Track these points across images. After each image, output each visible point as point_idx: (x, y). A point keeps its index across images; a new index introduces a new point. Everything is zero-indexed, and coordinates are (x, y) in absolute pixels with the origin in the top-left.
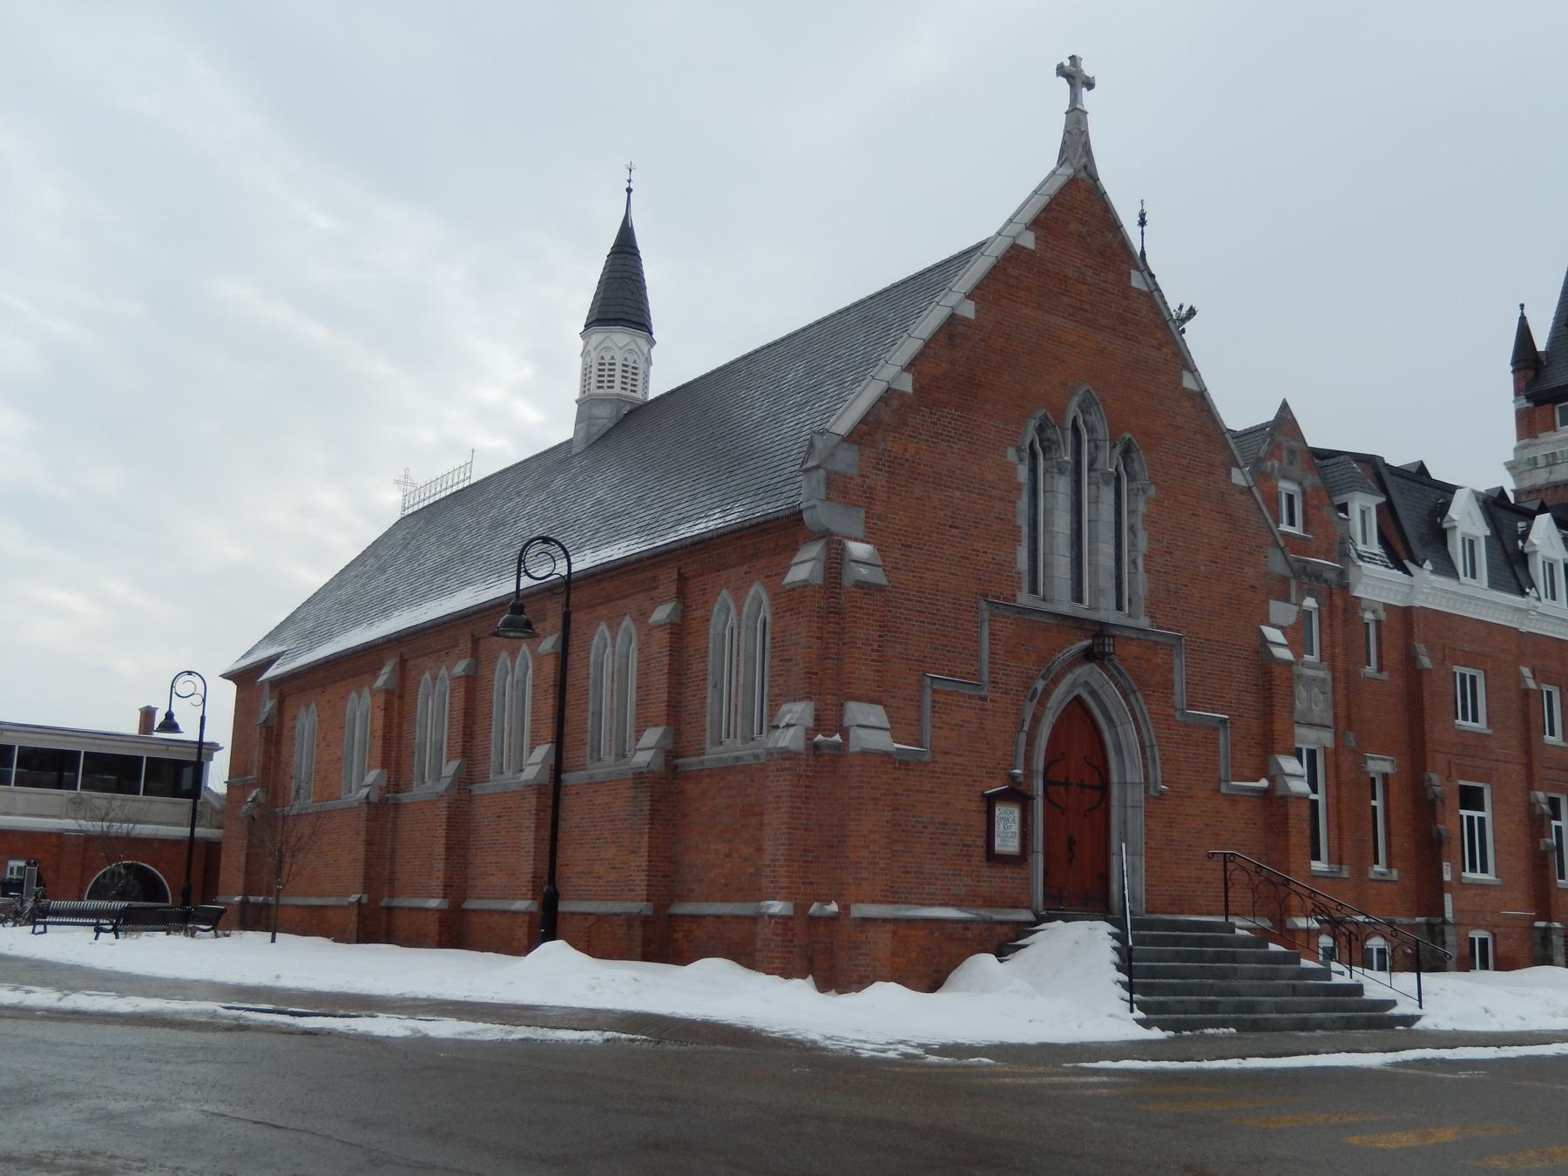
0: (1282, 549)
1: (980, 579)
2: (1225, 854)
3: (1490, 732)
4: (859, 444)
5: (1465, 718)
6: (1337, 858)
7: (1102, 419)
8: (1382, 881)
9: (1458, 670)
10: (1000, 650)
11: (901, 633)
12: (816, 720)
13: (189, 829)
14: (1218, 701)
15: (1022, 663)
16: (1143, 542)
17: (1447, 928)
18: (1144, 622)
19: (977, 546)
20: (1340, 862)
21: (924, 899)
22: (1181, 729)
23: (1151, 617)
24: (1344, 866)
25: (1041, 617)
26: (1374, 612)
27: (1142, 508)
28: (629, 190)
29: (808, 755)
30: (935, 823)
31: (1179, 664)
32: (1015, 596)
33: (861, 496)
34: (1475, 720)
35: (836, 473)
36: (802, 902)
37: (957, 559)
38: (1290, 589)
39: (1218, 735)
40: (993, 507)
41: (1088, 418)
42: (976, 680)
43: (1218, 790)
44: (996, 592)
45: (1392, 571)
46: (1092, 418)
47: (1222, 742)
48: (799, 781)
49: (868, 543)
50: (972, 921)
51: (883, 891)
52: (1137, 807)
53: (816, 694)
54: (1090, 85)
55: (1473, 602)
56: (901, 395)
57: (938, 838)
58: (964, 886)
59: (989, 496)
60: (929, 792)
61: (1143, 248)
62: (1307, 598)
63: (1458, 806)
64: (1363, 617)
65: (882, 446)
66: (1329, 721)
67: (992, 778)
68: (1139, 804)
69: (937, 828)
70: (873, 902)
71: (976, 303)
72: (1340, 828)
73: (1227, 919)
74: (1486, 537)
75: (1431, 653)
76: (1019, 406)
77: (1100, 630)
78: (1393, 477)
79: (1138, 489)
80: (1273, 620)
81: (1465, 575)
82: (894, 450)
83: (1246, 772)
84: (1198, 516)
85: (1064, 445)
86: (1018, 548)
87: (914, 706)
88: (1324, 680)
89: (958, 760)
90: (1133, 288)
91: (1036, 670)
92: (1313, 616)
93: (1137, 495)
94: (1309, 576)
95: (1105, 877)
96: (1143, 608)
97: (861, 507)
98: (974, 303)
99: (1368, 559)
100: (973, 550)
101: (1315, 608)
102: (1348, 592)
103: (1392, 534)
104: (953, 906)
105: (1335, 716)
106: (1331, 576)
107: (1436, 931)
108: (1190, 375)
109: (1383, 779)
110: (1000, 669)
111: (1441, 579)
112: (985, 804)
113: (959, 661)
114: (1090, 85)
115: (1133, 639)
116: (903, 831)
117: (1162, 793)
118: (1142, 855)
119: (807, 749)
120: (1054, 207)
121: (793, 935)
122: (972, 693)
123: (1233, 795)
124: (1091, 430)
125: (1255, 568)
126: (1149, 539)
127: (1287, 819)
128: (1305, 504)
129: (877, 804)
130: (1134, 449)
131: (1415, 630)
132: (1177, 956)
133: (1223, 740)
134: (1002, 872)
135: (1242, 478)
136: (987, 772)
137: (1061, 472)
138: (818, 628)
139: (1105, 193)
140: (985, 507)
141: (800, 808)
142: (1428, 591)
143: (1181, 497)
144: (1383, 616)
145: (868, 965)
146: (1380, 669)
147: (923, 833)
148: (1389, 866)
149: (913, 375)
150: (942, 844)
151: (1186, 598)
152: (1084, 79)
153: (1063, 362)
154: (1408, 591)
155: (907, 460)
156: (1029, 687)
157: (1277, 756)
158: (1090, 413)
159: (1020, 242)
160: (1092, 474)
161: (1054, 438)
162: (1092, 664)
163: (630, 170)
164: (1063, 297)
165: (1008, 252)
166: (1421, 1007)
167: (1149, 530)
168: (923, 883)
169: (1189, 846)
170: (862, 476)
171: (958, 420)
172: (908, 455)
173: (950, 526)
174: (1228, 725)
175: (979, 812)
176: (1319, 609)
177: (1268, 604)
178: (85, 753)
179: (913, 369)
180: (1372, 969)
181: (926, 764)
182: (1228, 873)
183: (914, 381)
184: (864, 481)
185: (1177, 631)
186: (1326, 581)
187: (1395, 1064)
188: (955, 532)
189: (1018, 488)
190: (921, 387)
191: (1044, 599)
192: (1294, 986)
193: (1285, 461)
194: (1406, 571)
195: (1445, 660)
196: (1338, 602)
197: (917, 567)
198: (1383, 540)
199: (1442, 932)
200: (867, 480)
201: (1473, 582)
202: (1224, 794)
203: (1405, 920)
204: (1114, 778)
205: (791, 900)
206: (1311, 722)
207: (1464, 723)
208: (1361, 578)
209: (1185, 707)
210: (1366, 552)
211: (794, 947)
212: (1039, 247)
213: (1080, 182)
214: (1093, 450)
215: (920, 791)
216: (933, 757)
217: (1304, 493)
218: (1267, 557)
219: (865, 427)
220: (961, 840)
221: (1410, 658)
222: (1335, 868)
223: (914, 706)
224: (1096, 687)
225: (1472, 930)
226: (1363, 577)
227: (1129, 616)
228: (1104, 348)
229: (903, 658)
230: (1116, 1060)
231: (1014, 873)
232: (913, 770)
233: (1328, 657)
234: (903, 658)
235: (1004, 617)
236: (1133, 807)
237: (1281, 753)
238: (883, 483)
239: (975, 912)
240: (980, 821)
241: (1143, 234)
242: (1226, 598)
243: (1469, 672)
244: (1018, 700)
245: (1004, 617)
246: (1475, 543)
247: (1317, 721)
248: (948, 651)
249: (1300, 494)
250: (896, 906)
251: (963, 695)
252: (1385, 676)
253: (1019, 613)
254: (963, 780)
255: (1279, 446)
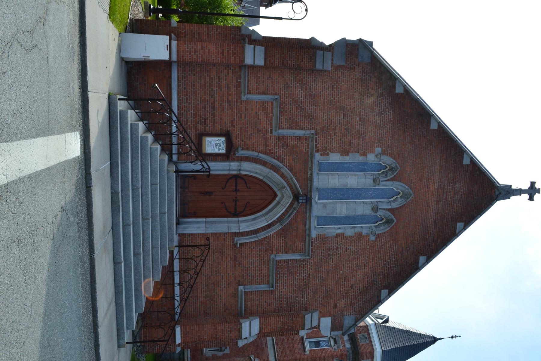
1: (323, 131)
7: (400, 204)
10: (294, 143)
15: (289, 155)
18: (314, 234)
22: (267, 259)
30: (214, 102)
32: (318, 152)
37: (330, 117)
39: (265, 284)
40: (355, 139)
44: (319, 140)
46: (399, 200)
47: (263, 286)
54: (531, 198)
69: (212, 104)
80: (322, 319)
86: (339, 154)
87: (265, 91)
89: (243, 115)
90: (457, 224)
91: (286, 164)
110: (285, 142)
114: (531, 198)
115: (305, 226)
122: (273, 125)
123: (238, 294)
125: (345, 307)
126: (351, 236)
129: (221, 54)
130: (389, 225)
135: (384, 297)
136: (239, 133)
141: (217, 32)
143: (372, 256)
147: (210, 95)
149: (403, 94)
150: (205, 107)
161: (388, 175)
162: (292, 197)
168: (187, 95)
170: (359, 64)
172: (370, 90)
177: (329, 317)
181: (240, 98)
182: (200, 247)
202: (238, 289)
204: (241, 219)
211: (158, 27)
215: (228, 94)
223: (265, 91)
224: (282, 202)
229: (285, 85)
234: (285, 85)
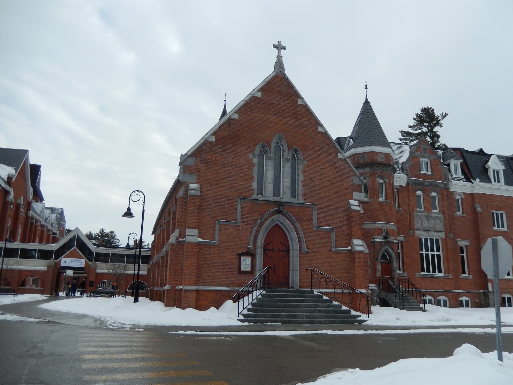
0: (358, 176)
2: (311, 270)
3: (508, 231)
4: (196, 157)
5: (498, 226)
6: (447, 272)
8: (466, 279)
9: (495, 212)
11: (209, 209)
12: (180, 234)
13: (133, 271)
14: (331, 223)
16: (301, 178)
17: (489, 294)
18: (302, 201)
19: (237, 182)
20: (449, 273)
21: (216, 284)
23: (304, 199)
24: (450, 275)
25: (261, 202)
26: (460, 195)
27: (301, 167)
28: (225, 100)
29: (177, 244)
31: (315, 213)
32: (251, 196)
33: (196, 171)
34: (503, 227)
35: (187, 165)
36: (173, 286)
38: (362, 188)
39: (331, 234)
41: (281, 143)
42: (236, 221)
43: (331, 251)
45: (466, 182)
46: (282, 143)
48: (173, 251)
49: (197, 184)
50: (232, 291)
51: (193, 282)
52: (297, 256)
53: (180, 227)
54: (284, 48)
55: (498, 190)
56: (211, 142)
57: (220, 267)
58: (230, 280)
59: (242, 168)
60: (217, 254)
61: (366, 95)
62: (433, 193)
63: (460, 253)
64: (455, 197)
65: (204, 157)
66: (443, 229)
67: (241, 249)
68: (297, 255)
69: (220, 264)
70: (190, 285)
71: (239, 114)
72: (448, 262)
73: (311, 290)
74: (503, 169)
75: (482, 207)
76: (254, 142)
77: (281, 204)
78: (468, 154)
79: (300, 162)
80: (354, 198)
81: (495, 181)
82: (208, 158)
83: (343, 245)
84: (324, 169)
85: (270, 152)
86: (253, 182)
88: (440, 217)
89: (228, 244)
90: (299, 104)
92: (459, 200)
93: (299, 164)
94: (433, 186)
95: (287, 278)
96: (301, 197)
97: (196, 174)
98: (238, 114)
99: (456, 180)
100: (236, 184)
101: (422, 194)
102: (449, 190)
103: (466, 171)
104: (226, 286)
105: (445, 228)
106: (442, 186)
107: (486, 295)
108: (321, 127)
109: (466, 247)
111: (484, 184)
112: (238, 256)
113: (229, 216)
114: (284, 48)
115: (297, 206)
116: (208, 265)
117: (307, 252)
118: (298, 271)
119: (176, 243)
120: (269, 84)
121: (170, 295)
122: (234, 225)
124: (283, 147)
126: (304, 176)
127: (355, 259)
128: (431, 164)
130: (298, 151)
131: (475, 200)
132: (280, 301)
133: (333, 235)
134: (244, 276)
137: (270, 159)
138: (181, 209)
139: (288, 78)
140: (241, 171)
142: (479, 188)
144: (463, 197)
145: (187, 303)
146: (463, 213)
148: (469, 274)
149: (215, 136)
150: (222, 268)
151: (319, 193)
152: (282, 47)
153: (271, 128)
154: (472, 188)
155: (213, 160)
156: (256, 222)
157: (353, 239)
158: (281, 142)
159: (256, 95)
160: (283, 159)
161: (267, 150)
163: (225, 95)
164: (272, 109)
165: (251, 98)
166: (369, 317)
167: (304, 174)
169: (318, 268)
171: (231, 148)
172: (213, 159)
173: (227, 177)
174: (334, 230)
175: (236, 259)
176: (438, 196)
177: (353, 193)
178: (95, 253)
179: (215, 134)
180: (441, 306)
181: (217, 245)
183: (216, 138)
184: (197, 167)
185: (314, 203)
186: (440, 187)
187: (296, 336)
188: (230, 179)
189: (253, 165)
190: (218, 139)
191: (264, 197)
192: (319, 310)
193: (423, 152)
194: (471, 182)
195: (488, 209)
196: (445, 193)
197: (215, 190)
198: (463, 172)
199: (488, 295)
200: (198, 167)
201: (499, 184)
202: (333, 252)
203: (475, 291)
204: (291, 248)
205: (170, 285)
206: (436, 230)
207: (498, 228)
208: (452, 185)
209: (316, 226)
210: (456, 177)
212: (262, 96)
213: (279, 76)
214: (283, 152)
215: (215, 253)
216: (219, 243)
217: (431, 161)
218: (352, 179)
219: (197, 152)
220: (229, 267)
221: (474, 209)
222: (447, 275)
224: (282, 221)
225: (503, 294)
226: (453, 185)
227: (297, 200)
228: (287, 123)
230: (241, 332)
231: (249, 277)
232: (212, 247)
233: (442, 210)
234: (209, 216)
235: (247, 202)
236: (296, 256)
237: (354, 238)
238: (204, 167)
239: (233, 288)
240: (236, 261)
241: (366, 91)
242: (335, 192)
243: (499, 212)
244: (251, 226)
245: (247, 202)
246: (499, 172)
247: (438, 230)
248: (226, 213)
249: (430, 162)
250: (205, 286)
251: (230, 225)
252: (465, 215)
253: (252, 201)
254: (230, 250)
255: (420, 148)
